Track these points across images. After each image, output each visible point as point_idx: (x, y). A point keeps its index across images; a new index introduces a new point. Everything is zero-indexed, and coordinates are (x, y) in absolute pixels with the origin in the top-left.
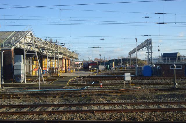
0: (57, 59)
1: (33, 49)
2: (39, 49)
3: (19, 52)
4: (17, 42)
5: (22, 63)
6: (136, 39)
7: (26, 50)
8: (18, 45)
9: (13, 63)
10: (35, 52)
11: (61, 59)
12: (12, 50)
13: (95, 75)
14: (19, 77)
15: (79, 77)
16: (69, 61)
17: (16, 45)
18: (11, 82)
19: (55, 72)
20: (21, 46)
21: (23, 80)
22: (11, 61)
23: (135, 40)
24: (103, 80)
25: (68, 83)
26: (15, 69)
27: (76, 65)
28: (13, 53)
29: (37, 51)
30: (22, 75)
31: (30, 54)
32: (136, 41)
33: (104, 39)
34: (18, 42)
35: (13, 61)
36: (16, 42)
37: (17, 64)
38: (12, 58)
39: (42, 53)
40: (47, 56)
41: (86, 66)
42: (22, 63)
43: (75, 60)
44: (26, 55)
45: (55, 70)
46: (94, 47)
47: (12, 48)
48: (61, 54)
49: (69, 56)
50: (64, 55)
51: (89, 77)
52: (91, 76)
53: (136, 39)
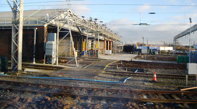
0: (97, 40)
1: (66, 26)
2: (78, 27)
3: (52, 29)
4: (52, 19)
5: (54, 43)
6: (190, 19)
7: (60, 28)
8: (53, 22)
9: (45, 41)
10: (69, 30)
11: (103, 41)
12: (45, 27)
13: (137, 60)
14: (49, 59)
15: (120, 62)
16: (111, 43)
17: (51, 22)
18: (43, 62)
19: (94, 54)
20: (56, 23)
21: (55, 60)
22: (43, 39)
23: (189, 20)
24: (149, 68)
25: (106, 67)
26: (46, 48)
27: (118, 47)
28: (46, 31)
29: (71, 29)
30: (53, 56)
31: (63, 34)
32: (190, 21)
33: (154, 13)
34: (53, 19)
35: (45, 39)
36: (51, 18)
37: (48, 42)
38: (45, 36)
39: (81, 33)
40: (86, 37)
41: (129, 49)
42: (54, 43)
43: (117, 42)
44: (59, 32)
45: (95, 52)
46: (140, 24)
47: (46, 26)
48: (101, 35)
49: (110, 38)
50: (104, 35)
51: (131, 62)
52: (133, 60)
53: (190, 19)
